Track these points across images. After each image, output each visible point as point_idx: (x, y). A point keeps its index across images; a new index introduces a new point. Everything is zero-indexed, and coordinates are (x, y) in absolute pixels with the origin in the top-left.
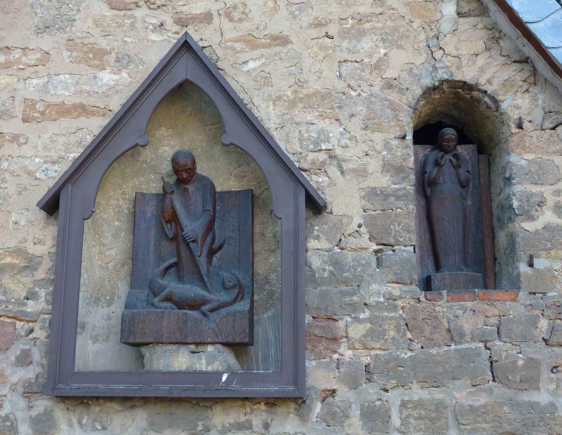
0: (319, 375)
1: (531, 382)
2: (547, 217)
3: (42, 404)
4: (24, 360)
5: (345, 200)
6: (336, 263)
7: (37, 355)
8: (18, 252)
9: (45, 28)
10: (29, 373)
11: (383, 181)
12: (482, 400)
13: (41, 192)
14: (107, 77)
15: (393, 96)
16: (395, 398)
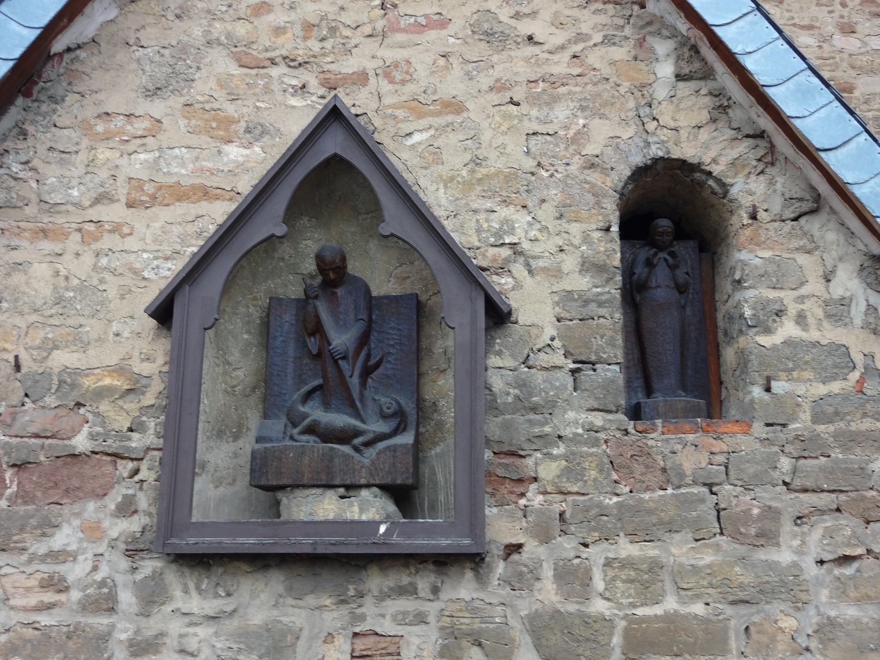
0: (501, 526)
1: (767, 537)
2: (788, 329)
3: (149, 566)
4: (127, 508)
5: (534, 306)
6: (522, 384)
7: (143, 502)
8: (120, 370)
9: (154, 92)
10: (133, 525)
11: (582, 283)
12: (708, 558)
13: (151, 294)
14: (234, 152)
15: (594, 177)
16: (597, 554)
